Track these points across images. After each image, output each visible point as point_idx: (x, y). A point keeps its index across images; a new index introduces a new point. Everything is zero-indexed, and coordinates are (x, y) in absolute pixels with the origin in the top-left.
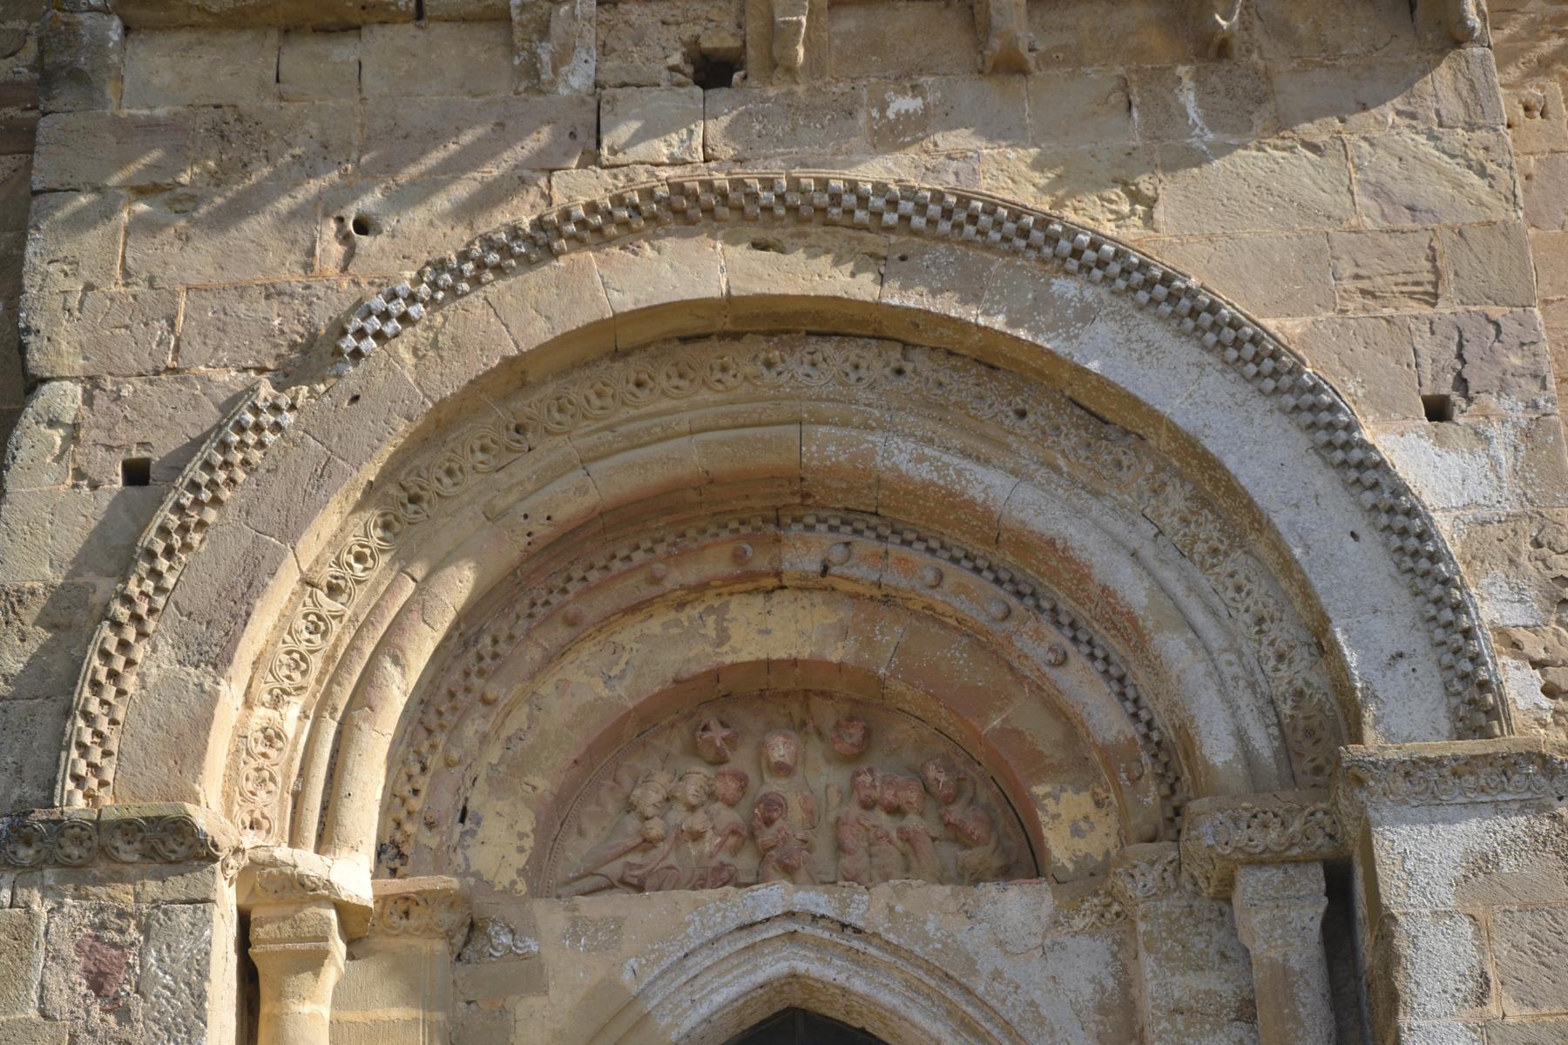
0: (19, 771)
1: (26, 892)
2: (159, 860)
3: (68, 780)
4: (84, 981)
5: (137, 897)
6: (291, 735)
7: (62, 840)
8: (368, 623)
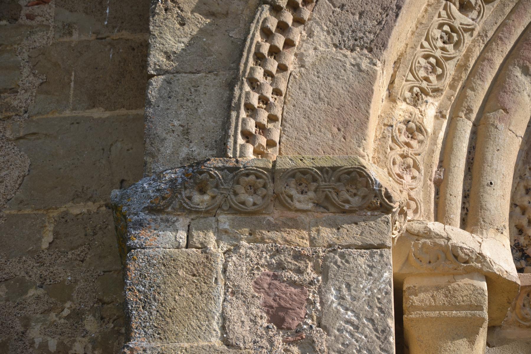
0: (186, 132)
1: (201, 234)
2: (332, 209)
3: (239, 136)
4: (265, 315)
5: (312, 241)
6: (430, 130)
7: (238, 188)
8: (497, 38)
